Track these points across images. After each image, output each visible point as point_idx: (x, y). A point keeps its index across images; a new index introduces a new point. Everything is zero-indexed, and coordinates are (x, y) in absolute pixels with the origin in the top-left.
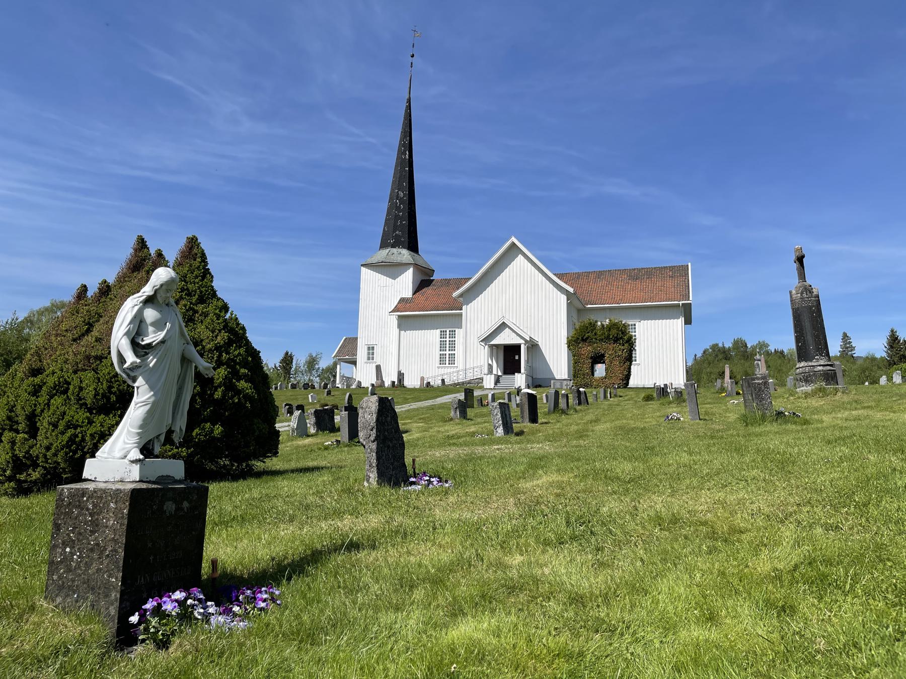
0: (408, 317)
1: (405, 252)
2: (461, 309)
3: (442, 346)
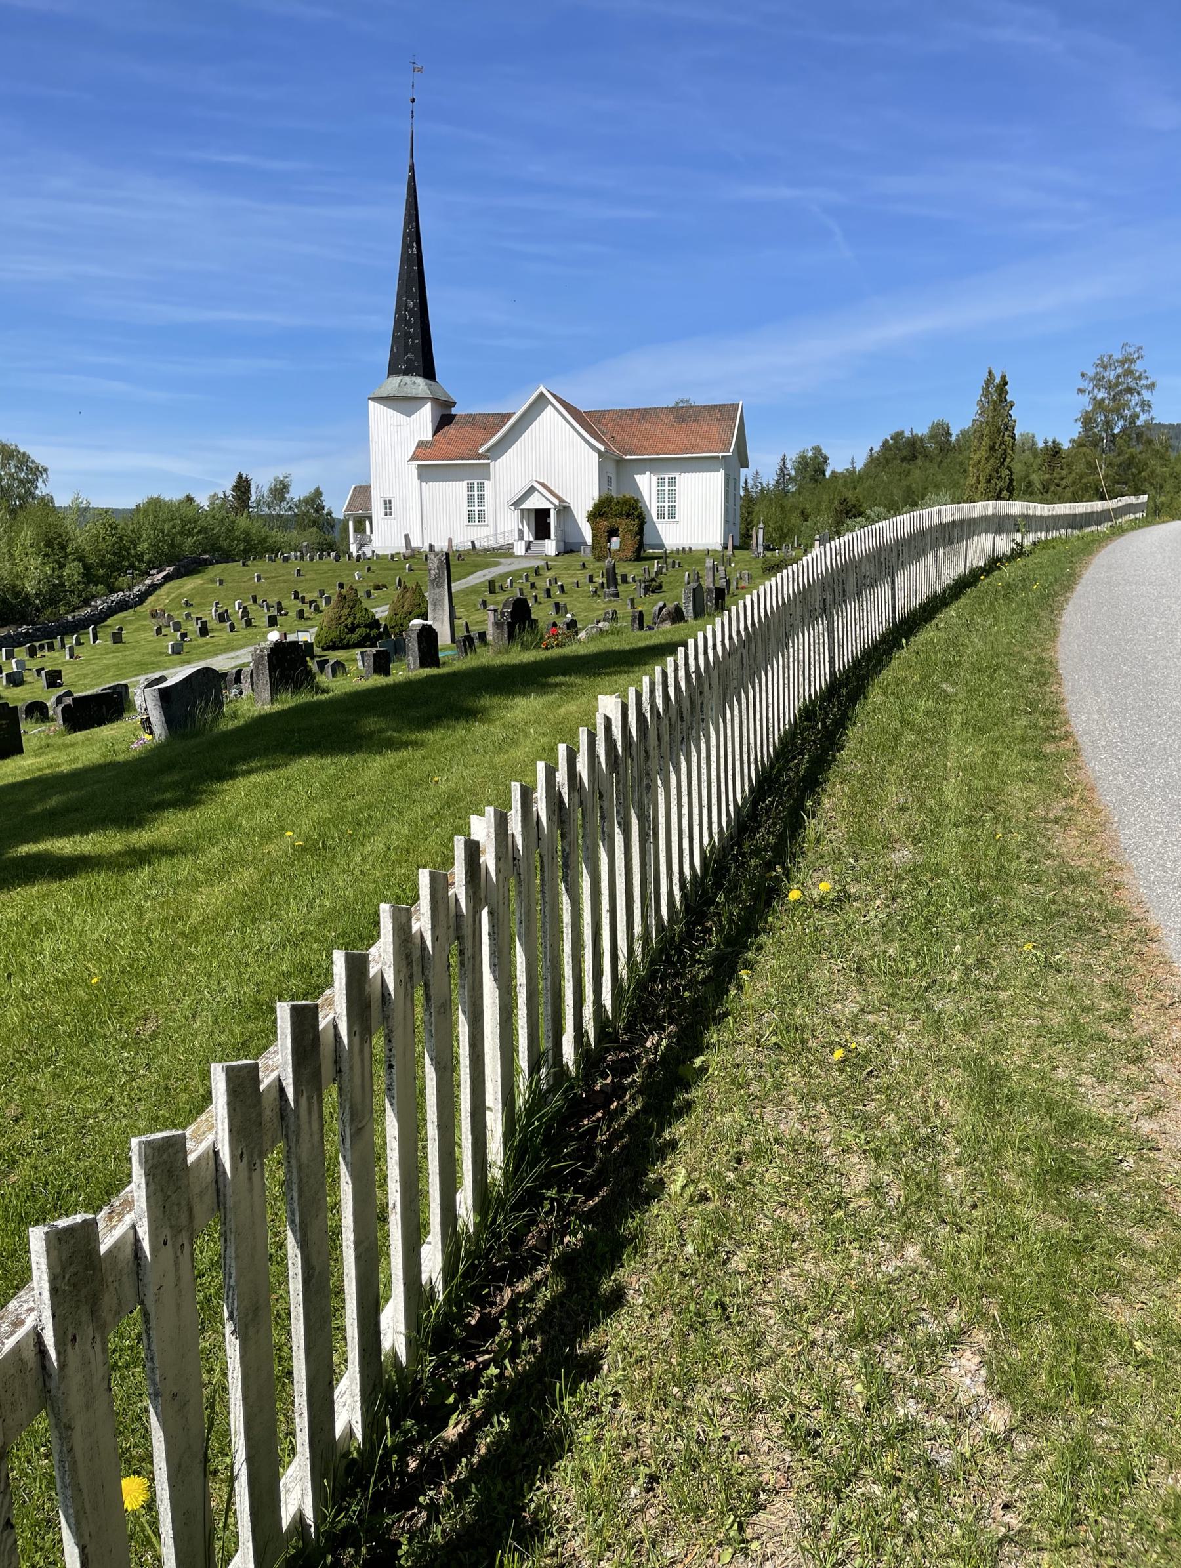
0: (432, 463)
1: (420, 380)
3: (470, 502)
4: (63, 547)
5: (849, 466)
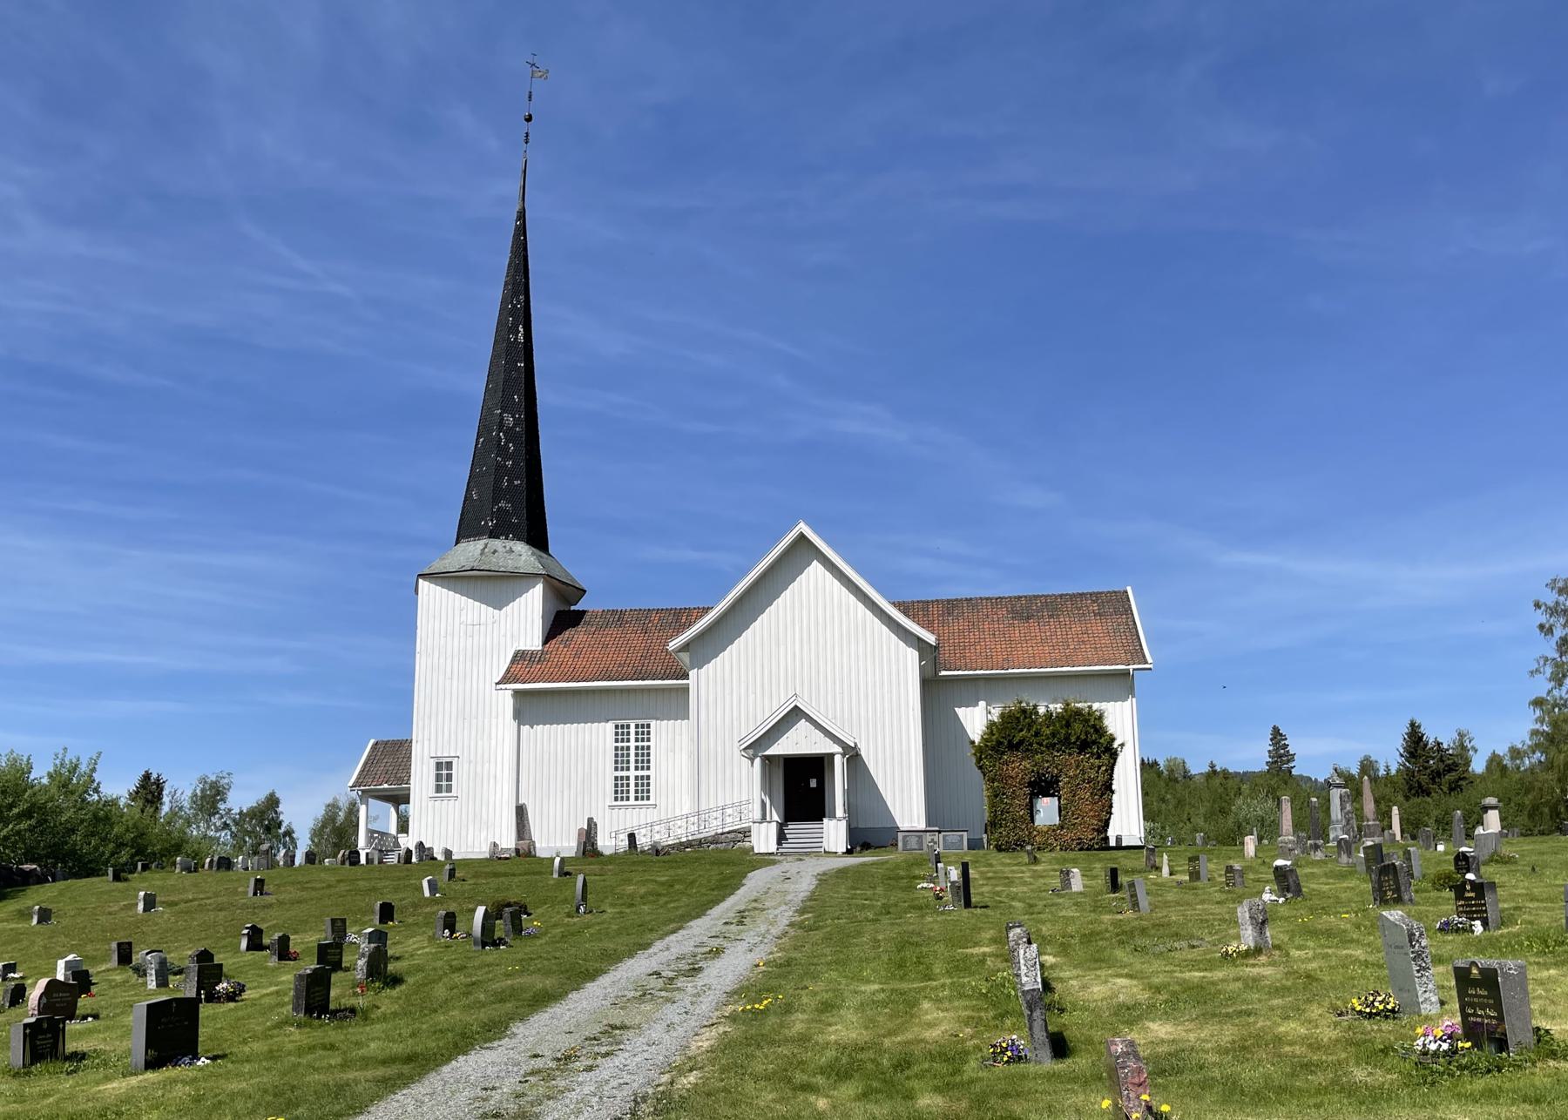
1: (521, 548)
2: (686, 676)
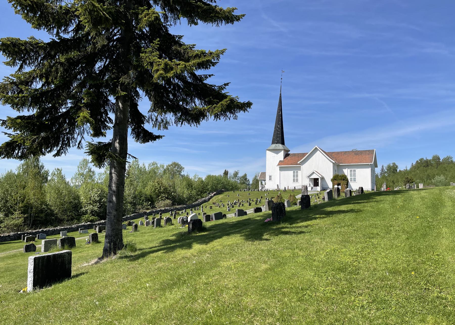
0: (283, 166)
1: (280, 145)
3: (294, 176)
4: (192, 186)
5: (405, 169)
